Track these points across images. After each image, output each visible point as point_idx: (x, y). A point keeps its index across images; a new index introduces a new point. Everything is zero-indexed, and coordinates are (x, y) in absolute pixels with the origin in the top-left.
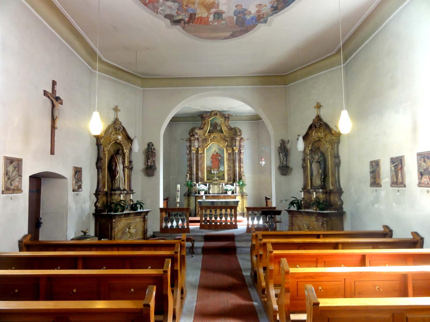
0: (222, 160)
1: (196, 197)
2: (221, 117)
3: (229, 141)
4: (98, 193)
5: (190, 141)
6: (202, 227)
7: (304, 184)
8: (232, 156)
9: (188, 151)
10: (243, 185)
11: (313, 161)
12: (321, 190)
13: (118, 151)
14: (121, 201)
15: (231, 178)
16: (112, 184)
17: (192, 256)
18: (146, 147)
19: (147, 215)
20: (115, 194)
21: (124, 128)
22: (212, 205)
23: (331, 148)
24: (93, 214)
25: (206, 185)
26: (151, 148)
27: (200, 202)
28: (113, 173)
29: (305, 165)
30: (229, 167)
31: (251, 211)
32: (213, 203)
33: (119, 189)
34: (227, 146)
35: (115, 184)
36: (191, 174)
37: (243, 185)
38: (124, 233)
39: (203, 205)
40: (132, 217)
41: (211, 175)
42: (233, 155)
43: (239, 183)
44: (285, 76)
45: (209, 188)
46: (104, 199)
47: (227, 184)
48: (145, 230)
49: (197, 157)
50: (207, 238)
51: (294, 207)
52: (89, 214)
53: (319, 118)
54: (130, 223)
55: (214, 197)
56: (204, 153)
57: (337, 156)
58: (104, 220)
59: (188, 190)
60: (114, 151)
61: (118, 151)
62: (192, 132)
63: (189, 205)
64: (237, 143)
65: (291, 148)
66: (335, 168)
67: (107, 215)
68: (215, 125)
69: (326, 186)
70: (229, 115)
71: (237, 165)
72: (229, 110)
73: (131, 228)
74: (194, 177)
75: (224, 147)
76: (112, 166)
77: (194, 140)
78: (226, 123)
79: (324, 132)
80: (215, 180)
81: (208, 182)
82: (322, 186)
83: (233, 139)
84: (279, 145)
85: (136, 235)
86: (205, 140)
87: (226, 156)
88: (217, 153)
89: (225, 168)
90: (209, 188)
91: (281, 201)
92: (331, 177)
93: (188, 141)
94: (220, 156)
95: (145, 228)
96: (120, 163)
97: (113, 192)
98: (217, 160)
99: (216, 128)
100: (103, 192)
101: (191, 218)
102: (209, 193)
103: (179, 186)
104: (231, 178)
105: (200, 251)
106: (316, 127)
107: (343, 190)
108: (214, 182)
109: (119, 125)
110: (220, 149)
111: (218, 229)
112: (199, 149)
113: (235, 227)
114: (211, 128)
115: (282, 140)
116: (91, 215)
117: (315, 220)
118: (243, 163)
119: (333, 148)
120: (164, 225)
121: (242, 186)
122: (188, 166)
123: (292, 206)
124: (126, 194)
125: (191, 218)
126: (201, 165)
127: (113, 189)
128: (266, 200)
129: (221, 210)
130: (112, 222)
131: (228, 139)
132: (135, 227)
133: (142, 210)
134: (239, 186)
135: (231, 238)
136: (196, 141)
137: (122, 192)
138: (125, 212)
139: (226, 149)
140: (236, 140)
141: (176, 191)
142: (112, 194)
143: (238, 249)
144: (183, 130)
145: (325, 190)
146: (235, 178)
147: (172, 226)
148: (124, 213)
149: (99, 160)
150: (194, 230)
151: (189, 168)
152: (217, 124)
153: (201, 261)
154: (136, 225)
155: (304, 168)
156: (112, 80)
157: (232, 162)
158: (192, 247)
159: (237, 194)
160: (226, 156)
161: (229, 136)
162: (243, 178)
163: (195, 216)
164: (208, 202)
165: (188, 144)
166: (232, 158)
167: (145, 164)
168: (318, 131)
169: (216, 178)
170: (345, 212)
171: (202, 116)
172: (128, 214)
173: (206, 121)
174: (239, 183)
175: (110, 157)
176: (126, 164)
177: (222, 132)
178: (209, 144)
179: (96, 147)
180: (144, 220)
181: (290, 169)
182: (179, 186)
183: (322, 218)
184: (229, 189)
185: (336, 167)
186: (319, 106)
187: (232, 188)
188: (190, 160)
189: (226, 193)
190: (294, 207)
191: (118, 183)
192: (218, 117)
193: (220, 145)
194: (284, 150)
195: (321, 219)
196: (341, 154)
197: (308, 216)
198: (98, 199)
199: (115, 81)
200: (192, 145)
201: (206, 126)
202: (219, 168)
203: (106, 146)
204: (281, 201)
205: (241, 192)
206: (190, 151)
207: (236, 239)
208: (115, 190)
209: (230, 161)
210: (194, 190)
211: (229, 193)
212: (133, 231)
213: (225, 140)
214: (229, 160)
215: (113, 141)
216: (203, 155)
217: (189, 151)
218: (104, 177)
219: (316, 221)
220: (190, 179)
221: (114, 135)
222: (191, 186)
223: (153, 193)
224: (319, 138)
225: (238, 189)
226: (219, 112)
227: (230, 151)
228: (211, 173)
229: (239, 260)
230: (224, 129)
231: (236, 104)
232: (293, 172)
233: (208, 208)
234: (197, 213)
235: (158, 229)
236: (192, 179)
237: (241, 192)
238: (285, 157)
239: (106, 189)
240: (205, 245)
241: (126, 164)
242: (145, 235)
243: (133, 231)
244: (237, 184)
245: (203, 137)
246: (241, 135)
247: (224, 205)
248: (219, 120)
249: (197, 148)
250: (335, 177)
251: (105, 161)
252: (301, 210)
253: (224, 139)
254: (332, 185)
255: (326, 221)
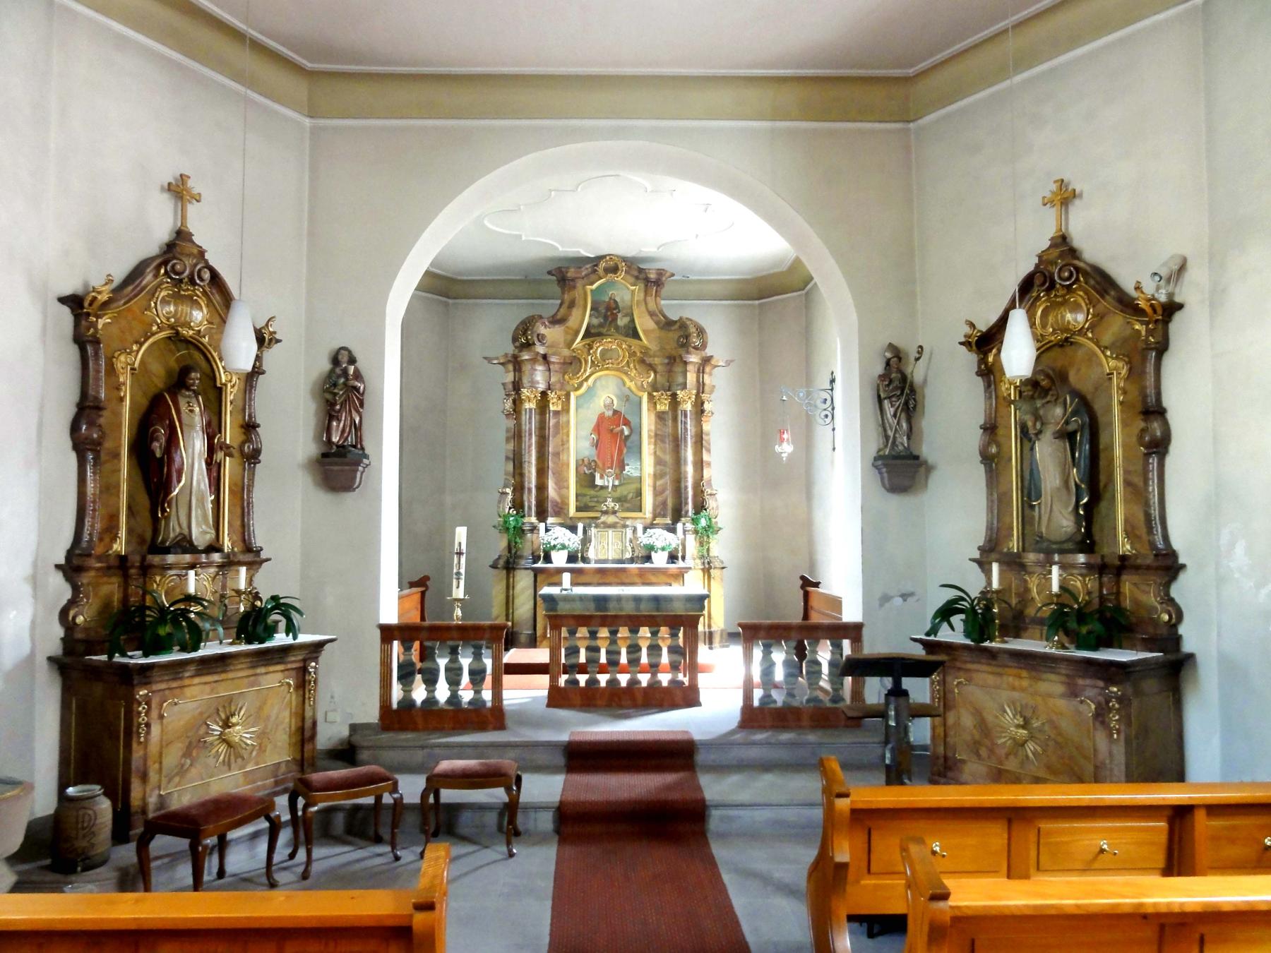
0: (634, 437)
1: (537, 572)
2: (632, 280)
3: (659, 368)
4: (75, 562)
5: (517, 364)
6: (557, 698)
7: (990, 528)
8: (670, 423)
9: (509, 405)
10: (710, 529)
11: (1040, 432)
12: (1081, 558)
13: (185, 371)
14: (190, 599)
15: (664, 503)
16: (156, 521)
17: (511, 855)
18: (326, 366)
19: (316, 659)
20: (165, 568)
21: (215, 276)
22: (598, 609)
23: (1124, 372)
24: (51, 659)
25: (573, 529)
26: (345, 371)
27: (550, 599)
28: (155, 475)
29: (994, 450)
30: (659, 462)
31: (752, 633)
32: (601, 601)
33: (184, 544)
34: (655, 387)
35: (167, 519)
36: (519, 489)
37: (710, 529)
38: (195, 745)
39: (563, 609)
40: (240, 672)
41: (592, 492)
42: (675, 419)
43: (695, 521)
44: (906, 80)
45: (586, 541)
46: (111, 588)
47: (651, 526)
48: (308, 724)
49: (542, 427)
50: (582, 757)
51: (952, 628)
52: (31, 657)
53: (1063, 245)
54: (230, 699)
55: (603, 576)
56: (566, 409)
57: (1154, 411)
58: (98, 689)
59: (509, 548)
60: (169, 373)
61: (185, 371)
62: (525, 333)
63: (509, 601)
64: (691, 378)
65: (925, 381)
66: (1146, 464)
67: (110, 664)
68: (608, 308)
69: (1097, 538)
70: (661, 273)
71: (689, 454)
72: (663, 253)
73: (234, 720)
74: (531, 500)
75: (642, 388)
76: (154, 439)
77: (534, 361)
78: (651, 300)
79: (1091, 302)
80: (605, 513)
81: (580, 519)
82: (1083, 542)
83: (675, 361)
84: (879, 369)
85: (262, 749)
86: (572, 364)
87: (648, 422)
88: (615, 412)
89: (645, 466)
90: (586, 541)
91: (885, 599)
92: (1126, 501)
93: (511, 367)
94: (627, 423)
95: (308, 714)
96: (192, 427)
97: (156, 559)
98: (615, 435)
99: (615, 319)
100: (102, 557)
101: (514, 656)
102: (585, 560)
103: (461, 534)
104: (664, 503)
105: (546, 822)
106: (1052, 286)
107: (1181, 560)
108: (603, 518)
109: (189, 262)
110: (627, 399)
111: (621, 707)
112: (551, 395)
113: (688, 697)
114: (595, 321)
115: (892, 347)
116: (41, 661)
117: (1059, 689)
118: (709, 451)
119: (1135, 373)
120: (397, 692)
121: (705, 534)
122: (507, 458)
123: (945, 625)
124: (221, 567)
125: (514, 656)
126: (557, 454)
127: (157, 544)
128: (803, 587)
129: (634, 631)
130: (131, 702)
131: (657, 361)
132: (257, 716)
133: (289, 640)
134: (696, 532)
135: (676, 754)
136: (540, 368)
137: (203, 558)
138: (209, 649)
139: (651, 397)
140: (686, 363)
141: (452, 553)
142: (151, 566)
143: (715, 816)
144: (490, 329)
145: (1096, 559)
146: (682, 503)
147: (430, 701)
148: (201, 653)
149: (88, 408)
150: (525, 718)
151: (510, 467)
152: (617, 307)
153: (548, 885)
154: (260, 708)
155: (992, 461)
156: (169, 60)
157: (668, 446)
158: (511, 809)
159: (689, 562)
160: (648, 422)
161: (662, 349)
162: (711, 503)
163: (533, 643)
164: (582, 598)
165: (510, 377)
166: (670, 430)
167: (318, 438)
168: (1065, 303)
169: (610, 504)
170: (1191, 657)
171: (565, 275)
172: (221, 662)
173: (577, 293)
174: (695, 521)
175: (144, 402)
176: (230, 434)
177: (635, 335)
178: (586, 379)
179: (73, 352)
180: (303, 682)
181: (922, 470)
182: (461, 534)
183: (1101, 684)
184: (658, 544)
185: (1148, 455)
186: (1065, 197)
187: (672, 540)
188: (517, 435)
189: (648, 558)
190: (952, 628)
191: (185, 525)
192: (620, 278)
193: (628, 383)
194: (897, 388)
195: (1091, 688)
196: (1171, 399)
197: (1024, 673)
198: (76, 589)
199: (180, 67)
200: (525, 381)
201: (576, 313)
202: (622, 466)
203: (124, 350)
204: (885, 599)
205: (702, 557)
206: (517, 403)
207: (700, 758)
208: (167, 551)
209: (663, 441)
210: (529, 544)
211: (660, 560)
212: (241, 733)
213: (645, 363)
214: (658, 437)
215: (160, 329)
216: (563, 419)
217: (514, 401)
218: (109, 489)
219: (1063, 696)
220: (514, 506)
221: (164, 302)
222: (520, 532)
223: (344, 565)
224: (1067, 330)
225: (691, 541)
226: (625, 259)
227: (663, 407)
228: (592, 484)
229: (726, 878)
230: (644, 323)
231: (695, 217)
232: (935, 480)
233: (583, 620)
234: (539, 633)
235: (372, 714)
236: (522, 506)
237: (702, 557)
238: (903, 415)
239: (120, 547)
240: (571, 797)
241: (230, 434)
242: (308, 747)
243: (241, 733)
244: (689, 526)
245: (566, 352)
246: (704, 346)
247: (645, 610)
248: (625, 291)
249: (544, 394)
250: (1147, 504)
251: (118, 414)
252: (987, 644)
253: (642, 361)
254: (1129, 534)
255: (1120, 700)
